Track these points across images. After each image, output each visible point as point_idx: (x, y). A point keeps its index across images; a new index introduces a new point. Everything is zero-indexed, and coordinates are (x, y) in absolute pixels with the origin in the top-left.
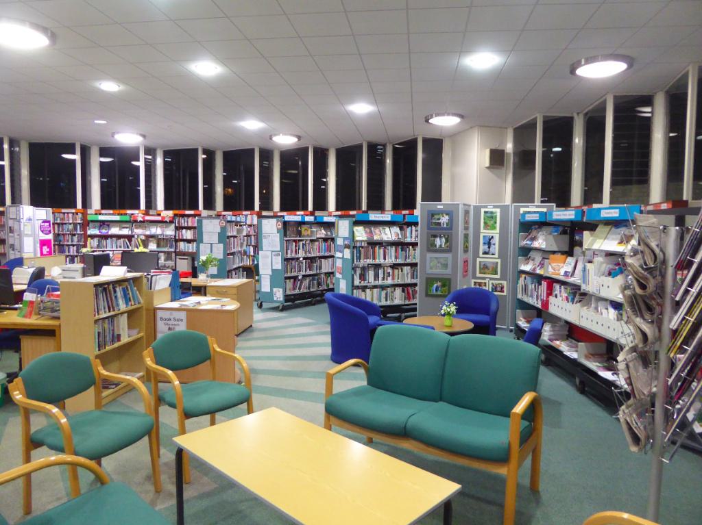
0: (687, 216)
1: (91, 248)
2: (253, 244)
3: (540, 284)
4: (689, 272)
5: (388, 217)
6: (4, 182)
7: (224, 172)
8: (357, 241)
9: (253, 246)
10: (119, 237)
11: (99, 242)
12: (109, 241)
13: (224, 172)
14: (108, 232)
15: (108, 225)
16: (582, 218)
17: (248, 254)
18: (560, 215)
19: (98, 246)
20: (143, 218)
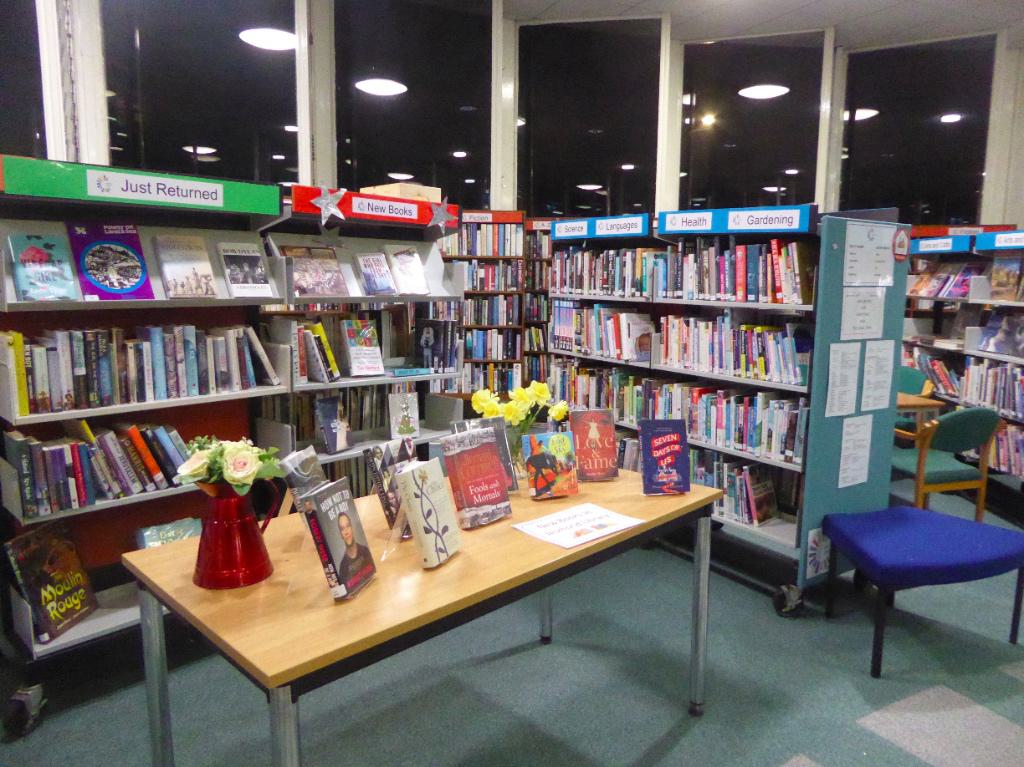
0: (516, 209)
1: (35, 406)
2: (502, 322)
3: (752, 403)
4: (689, 136)
5: (790, 220)
6: (525, 139)
7: (682, 170)
8: (556, 338)
9: (501, 331)
10: (209, 317)
11: (93, 357)
12: (153, 349)
13: (682, 170)
14: (145, 290)
15: (133, 243)
16: (971, 248)
17: (478, 356)
18: (771, 220)
19: (84, 391)
20: (344, 204)
